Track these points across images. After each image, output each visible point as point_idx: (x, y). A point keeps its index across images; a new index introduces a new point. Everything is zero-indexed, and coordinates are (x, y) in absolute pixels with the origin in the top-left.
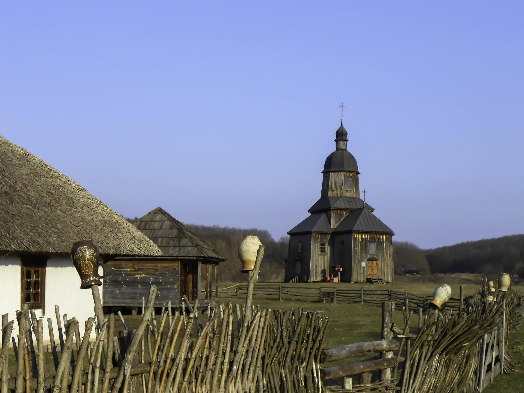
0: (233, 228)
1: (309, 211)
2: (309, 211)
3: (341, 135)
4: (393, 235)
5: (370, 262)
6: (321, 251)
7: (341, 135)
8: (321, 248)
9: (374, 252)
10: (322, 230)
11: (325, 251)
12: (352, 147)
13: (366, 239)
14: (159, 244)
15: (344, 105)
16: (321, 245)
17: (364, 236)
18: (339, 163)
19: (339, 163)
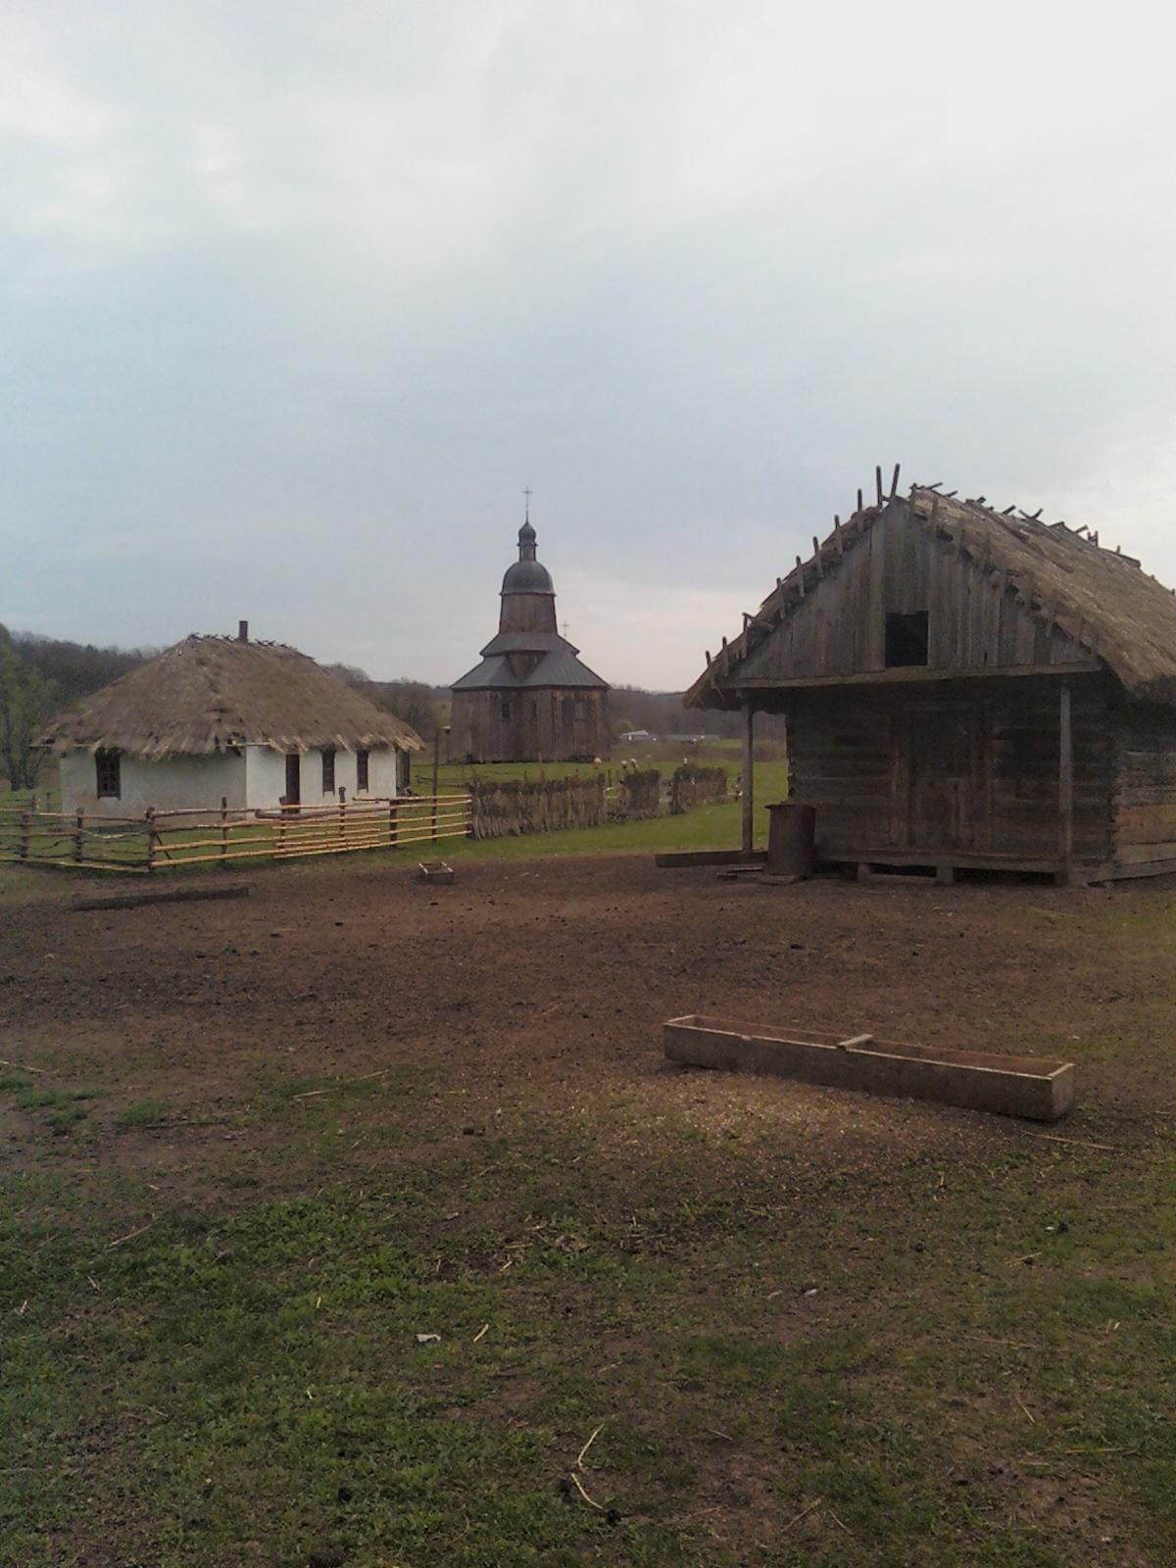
3: (527, 537)
6: (504, 716)
7: (527, 537)
12: (542, 557)
16: (503, 706)
17: (567, 693)
18: (527, 592)
19: (527, 592)
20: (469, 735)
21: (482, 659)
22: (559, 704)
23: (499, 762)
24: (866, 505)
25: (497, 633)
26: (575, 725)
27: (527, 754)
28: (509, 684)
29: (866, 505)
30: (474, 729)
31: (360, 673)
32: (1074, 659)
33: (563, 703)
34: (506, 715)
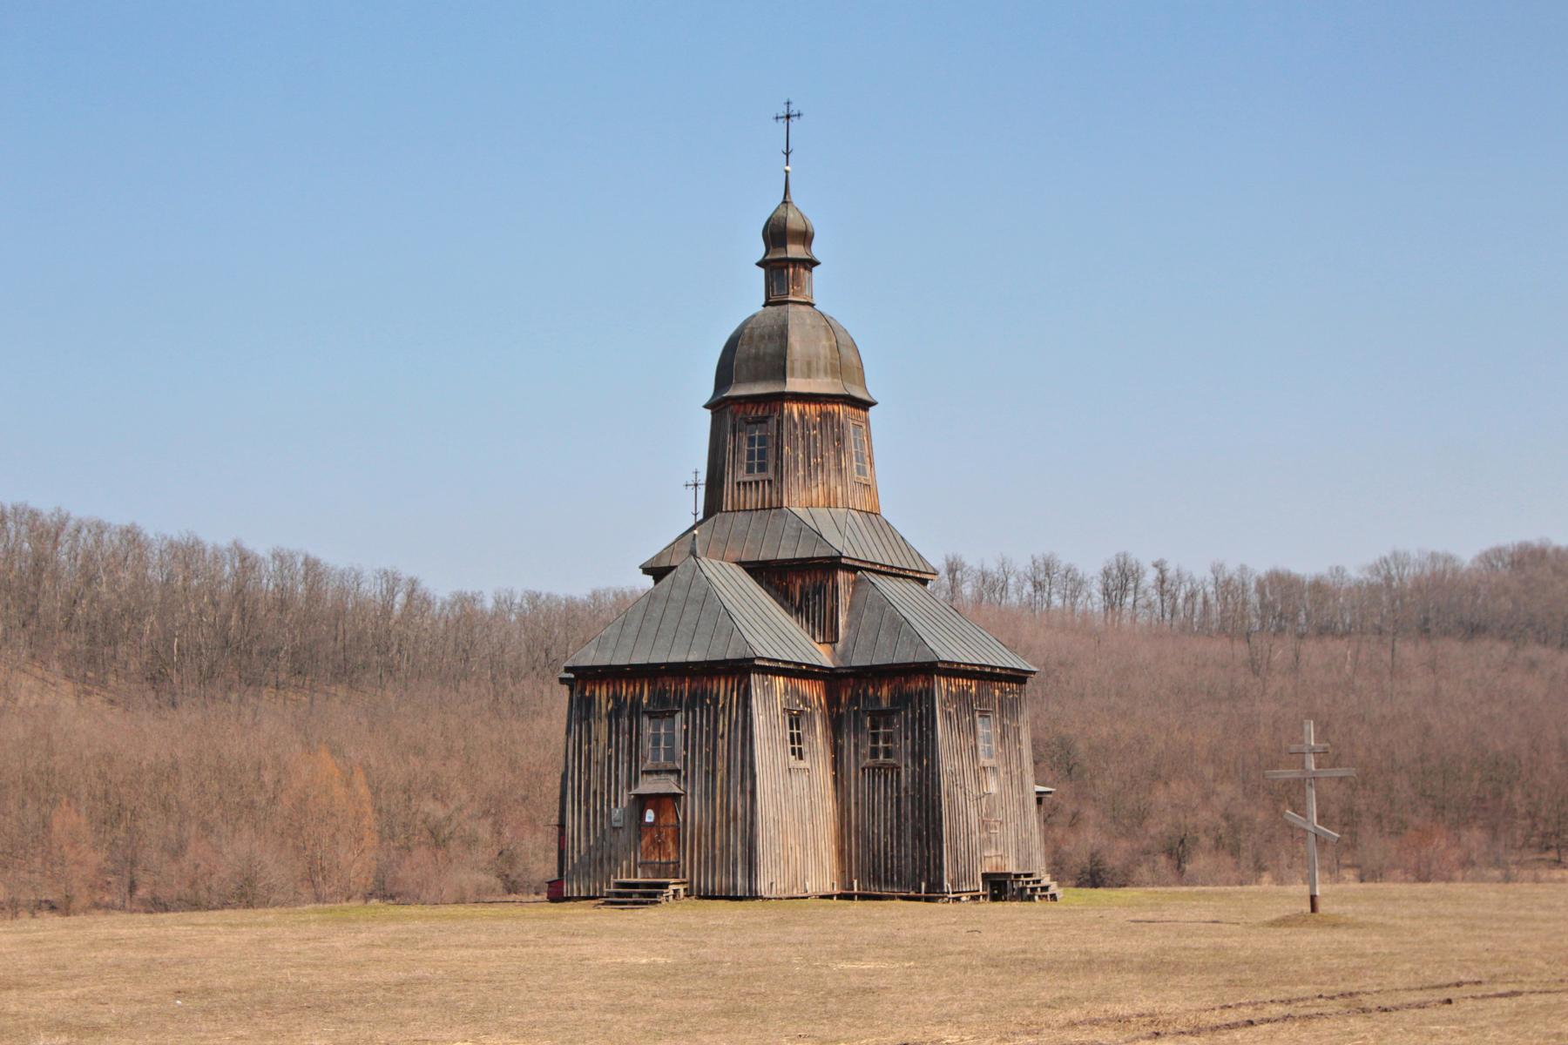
3: (785, 253)
7: (785, 253)
13: (636, 703)
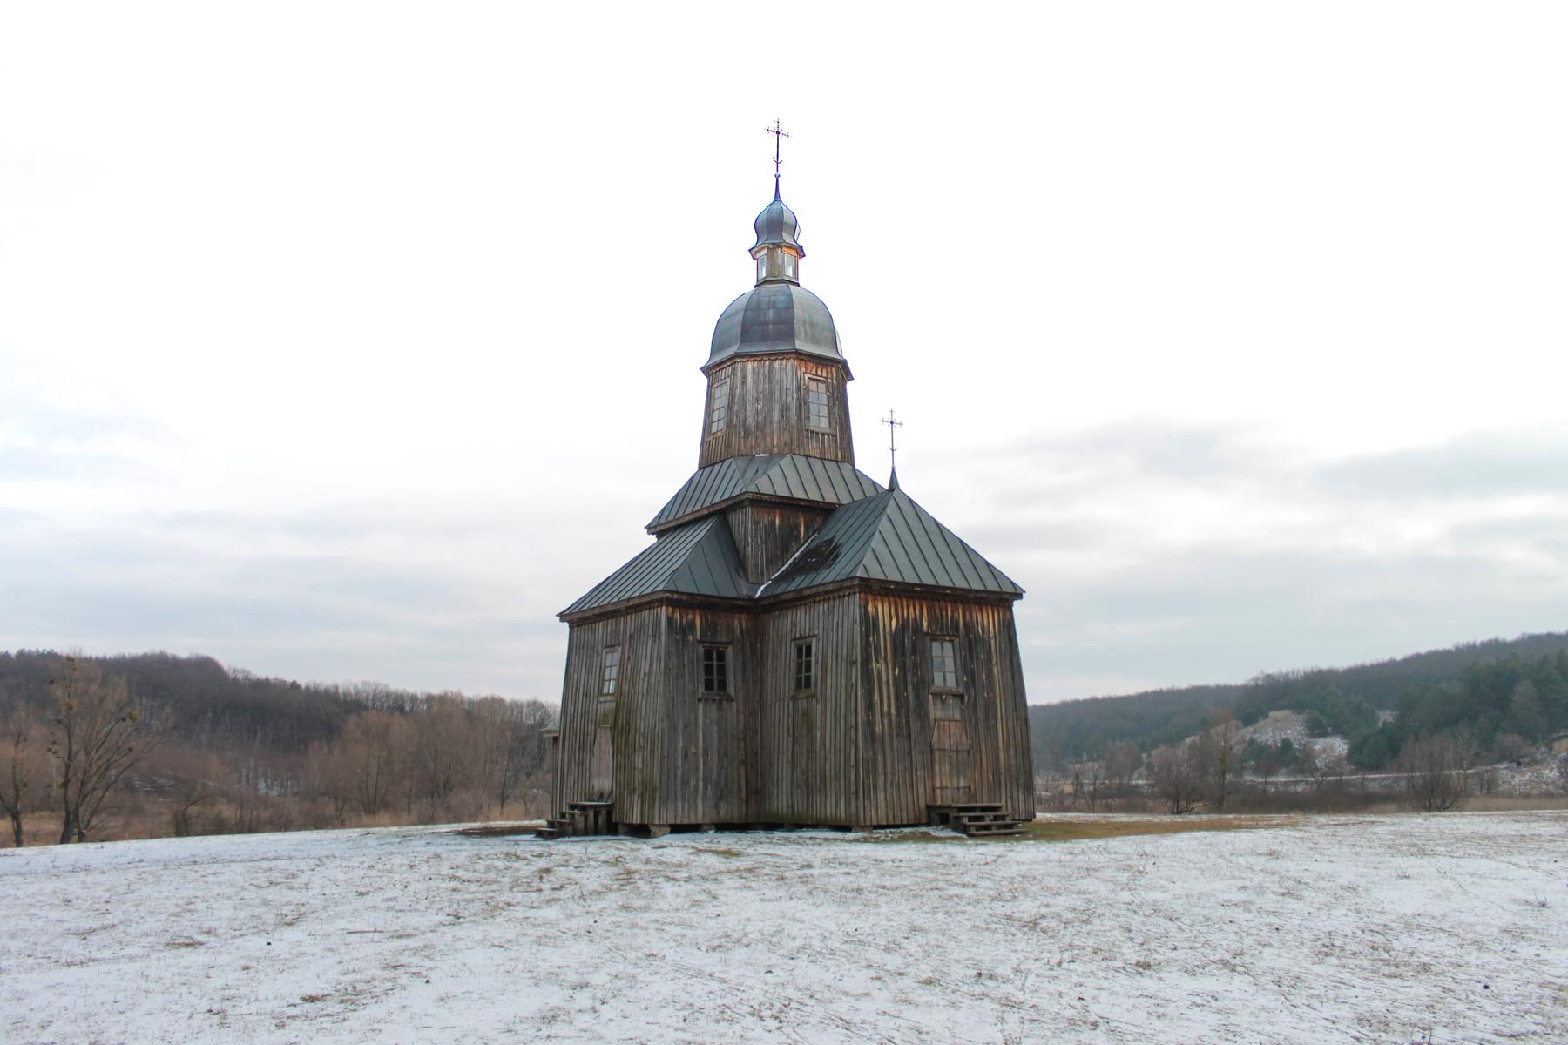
0: (21, 654)
1: (650, 528)
2: (650, 528)
3: (775, 231)
4: (1018, 594)
5: (23, 837)
6: (709, 685)
7: (775, 231)
8: (708, 670)
9: (951, 682)
10: (708, 589)
11: (723, 685)
12: (816, 277)
14: (293, 807)
15: (783, 129)
16: (708, 655)
17: (912, 611)
18: (775, 352)
19: (775, 352)
20: (604, 743)
21: (653, 539)
22: (885, 645)
23: (695, 828)
24: (776, 468)
25: (693, 467)
26: (935, 711)
27: (780, 804)
28: (728, 592)
29: (776, 468)
30: (621, 729)
31: (206, 667)
32: (549, 777)
33: (897, 637)
34: (715, 681)
